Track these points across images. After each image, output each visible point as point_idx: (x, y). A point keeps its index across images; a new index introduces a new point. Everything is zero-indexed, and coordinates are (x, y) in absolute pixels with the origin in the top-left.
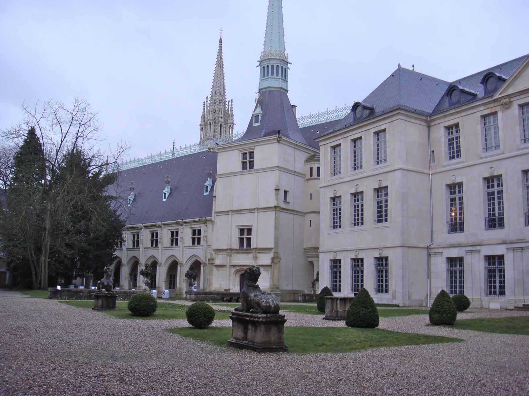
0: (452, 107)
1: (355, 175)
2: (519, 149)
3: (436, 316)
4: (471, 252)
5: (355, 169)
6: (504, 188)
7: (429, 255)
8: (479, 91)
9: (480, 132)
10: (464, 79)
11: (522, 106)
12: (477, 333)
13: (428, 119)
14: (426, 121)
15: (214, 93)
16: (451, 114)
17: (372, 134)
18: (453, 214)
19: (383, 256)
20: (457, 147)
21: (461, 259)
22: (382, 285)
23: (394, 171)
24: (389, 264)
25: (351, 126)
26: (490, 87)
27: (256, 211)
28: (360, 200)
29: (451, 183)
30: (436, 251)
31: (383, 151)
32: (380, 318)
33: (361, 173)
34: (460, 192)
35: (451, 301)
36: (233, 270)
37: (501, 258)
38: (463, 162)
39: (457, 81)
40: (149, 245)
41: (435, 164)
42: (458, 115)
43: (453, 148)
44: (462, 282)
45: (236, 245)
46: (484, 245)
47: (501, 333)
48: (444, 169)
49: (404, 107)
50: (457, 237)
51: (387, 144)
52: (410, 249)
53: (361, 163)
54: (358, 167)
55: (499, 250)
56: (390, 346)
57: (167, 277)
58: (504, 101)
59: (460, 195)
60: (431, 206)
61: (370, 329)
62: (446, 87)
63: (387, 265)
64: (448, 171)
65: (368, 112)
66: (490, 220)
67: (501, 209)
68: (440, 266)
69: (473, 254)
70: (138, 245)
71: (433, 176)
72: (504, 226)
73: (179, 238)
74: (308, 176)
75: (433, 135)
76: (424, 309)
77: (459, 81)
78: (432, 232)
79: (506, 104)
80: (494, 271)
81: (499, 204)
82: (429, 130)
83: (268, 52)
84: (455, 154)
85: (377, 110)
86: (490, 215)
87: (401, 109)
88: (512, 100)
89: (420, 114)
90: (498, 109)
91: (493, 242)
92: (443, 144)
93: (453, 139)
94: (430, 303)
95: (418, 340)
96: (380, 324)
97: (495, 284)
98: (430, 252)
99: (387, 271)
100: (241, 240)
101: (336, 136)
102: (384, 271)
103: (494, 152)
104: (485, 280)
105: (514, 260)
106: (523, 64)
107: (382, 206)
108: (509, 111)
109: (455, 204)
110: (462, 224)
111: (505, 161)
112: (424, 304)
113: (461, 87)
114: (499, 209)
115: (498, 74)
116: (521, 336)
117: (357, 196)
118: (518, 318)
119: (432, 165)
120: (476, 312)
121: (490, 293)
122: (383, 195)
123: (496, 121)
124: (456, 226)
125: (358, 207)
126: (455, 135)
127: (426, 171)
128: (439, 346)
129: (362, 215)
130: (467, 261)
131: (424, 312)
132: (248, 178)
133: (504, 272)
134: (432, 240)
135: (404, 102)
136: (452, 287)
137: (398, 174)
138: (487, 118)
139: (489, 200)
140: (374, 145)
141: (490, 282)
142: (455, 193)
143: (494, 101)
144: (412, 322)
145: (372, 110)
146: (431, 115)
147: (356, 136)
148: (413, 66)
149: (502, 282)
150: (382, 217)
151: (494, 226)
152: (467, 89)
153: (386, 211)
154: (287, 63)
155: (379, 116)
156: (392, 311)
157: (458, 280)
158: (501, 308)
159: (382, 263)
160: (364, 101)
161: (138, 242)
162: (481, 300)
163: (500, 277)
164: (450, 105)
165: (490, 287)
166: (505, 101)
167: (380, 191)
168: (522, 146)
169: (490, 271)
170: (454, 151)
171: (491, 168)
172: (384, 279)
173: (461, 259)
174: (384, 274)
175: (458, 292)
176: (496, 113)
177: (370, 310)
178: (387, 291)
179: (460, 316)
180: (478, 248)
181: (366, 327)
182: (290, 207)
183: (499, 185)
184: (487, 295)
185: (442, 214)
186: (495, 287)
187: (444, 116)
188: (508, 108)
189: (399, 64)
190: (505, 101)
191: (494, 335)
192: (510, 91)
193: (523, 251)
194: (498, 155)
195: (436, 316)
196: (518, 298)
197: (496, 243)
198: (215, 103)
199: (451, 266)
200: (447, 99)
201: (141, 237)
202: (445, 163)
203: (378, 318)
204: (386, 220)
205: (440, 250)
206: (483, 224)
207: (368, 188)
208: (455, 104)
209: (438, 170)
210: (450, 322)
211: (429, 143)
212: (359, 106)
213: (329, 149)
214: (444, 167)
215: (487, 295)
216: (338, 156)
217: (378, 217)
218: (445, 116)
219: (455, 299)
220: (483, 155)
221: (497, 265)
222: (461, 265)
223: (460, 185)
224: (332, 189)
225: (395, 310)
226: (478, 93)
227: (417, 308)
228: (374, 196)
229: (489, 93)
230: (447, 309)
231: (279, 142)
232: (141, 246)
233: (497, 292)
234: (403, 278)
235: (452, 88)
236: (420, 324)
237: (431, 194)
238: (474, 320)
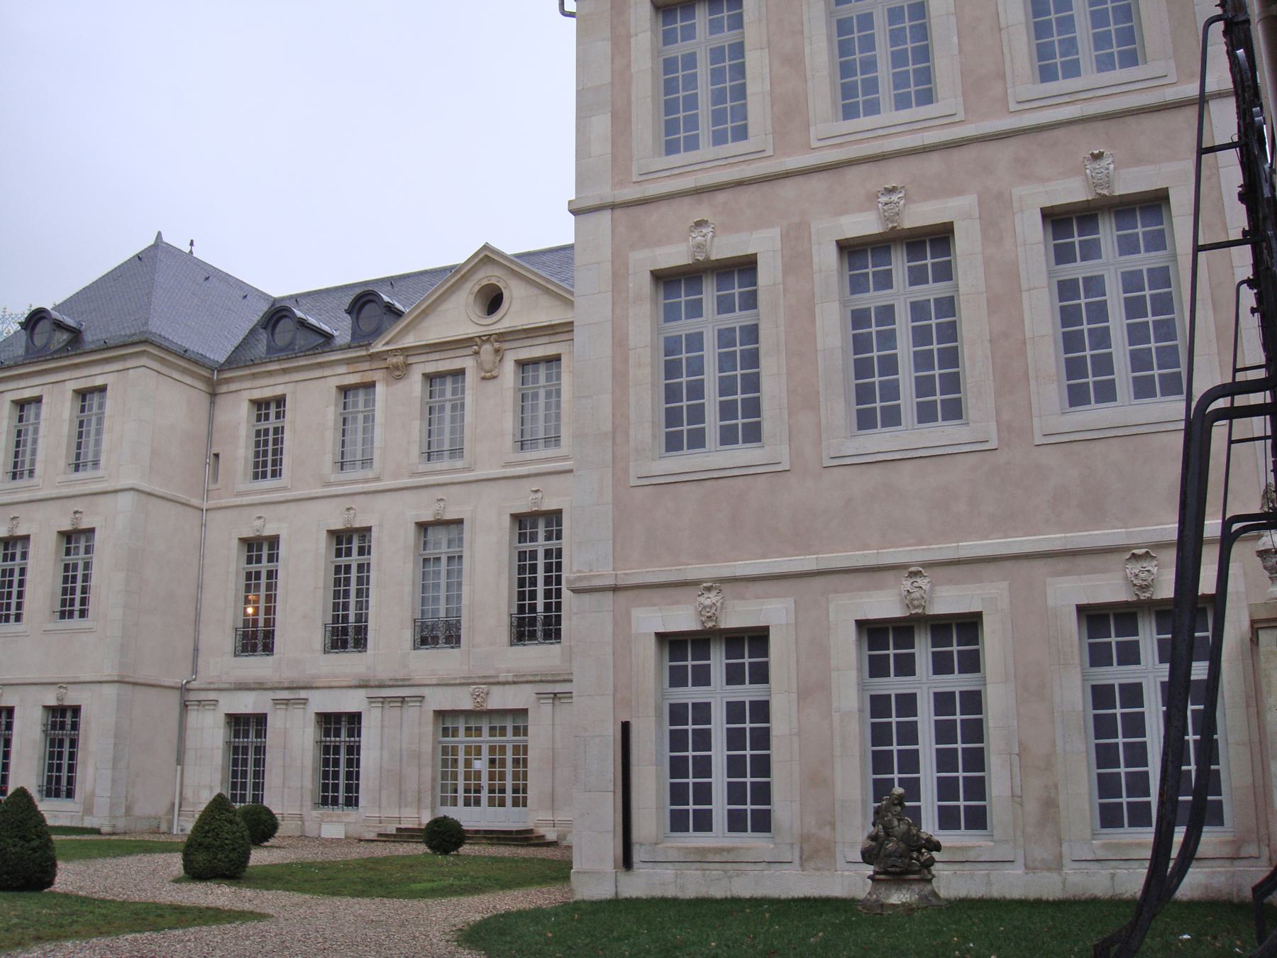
0: (274, 357)
2: (414, 474)
3: (201, 857)
4: (287, 702)
5: (14, 477)
6: (374, 558)
7: (185, 706)
8: (341, 328)
9: (331, 423)
10: (309, 294)
11: (430, 378)
12: (297, 897)
13: (212, 378)
14: (208, 381)
16: (270, 373)
17: (69, 394)
18: (250, 610)
19: (67, 703)
20: (275, 452)
21: (261, 719)
22: (59, 779)
23: (116, 491)
24: (82, 726)
25: (17, 365)
26: (366, 326)
28: (18, 556)
29: (251, 535)
31: (92, 442)
32: (61, 865)
34: (272, 558)
35: (238, 819)
37: (355, 718)
38: (285, 489)
39: (290, 297)
41: (218, 486)
42: (286, 378)
43: (265, 453)
44: (259, 774)
46: (317, 688)
47: (353, 896)
48: (239, 501)
49: (158, 340)
50: (256, 667)
51: (106, 423)
52: (138, 688)
53: (33, 462)
54: (22, 473)
56: (88, 936)
58: (393, 360)
59: (271, 566)
60: (200, 586)
61: (31, 894)
62: (264, 307)
63: (75, 726)
64: (246, 506)
65: (64, 337)
66: (335, 631)
67: (362, 605)
68: (209, 733)
69: (290, 707)
71: (211, 514)
72: (365, 646)
75: (222, 417)
76: (163, 838)
77: (296, 298)
78: (196, 650)
79: (396, 367)
80: (337, 750)
81: (359, 593)
82: (212, 403)
84: (269, 469)
85: (88, 337)
86: (336, 619)
87: (152, 343)
88: (411, 360)
89: (196, 363)
90: (377, 376)
91: (339, 682)
93: (266, 431)
94: (185, 825)
95: (160, 920)
96: (57, 879)
97: (338, 779)
98: (186, 698)
99: (73, 743)
102: (67, 744)
103: (359, 474)
104: (314, 770)
105: (382, 727)
106: (442, 285)
107: (74, 577)
108: (401, 385)
109: (258, 587)
110: (269, 635)
111: (380, 497)
112: (164, 828)
113: (299, 314)
114: (360, 605)
115: (386, 299)
116: (397, 903)
118: (386, 858)
119: (212, 487)
120: (291, 846)
121: (325, 801)
122: (82, 550)
123: (370, 403)
124: (256, 639)
125: (11, 574)
126: (272, 423)
127: (195, 501)
128: (211, 933)
129: (20, 595)
131: (167, 848)
133: (358, 754)
134: (195, 671)
135: (159, 326)
136: (234, 786)
137: (125, 500)
138: (351, 394)
139: (337, 582)
140: (71, 421)
141: (326, 775)
142: (259, 560)
143: (372, 357)
144: (137, 872)
145: (76, 335)
146: (221, 368)
147: (27, 394)
148: (192, 244)
149: (353, 776)
150: (72, 604)
151: (254, 649)
152: (312, 321)
156: (86, 843)
157: (250, 768)
158: (347, 837)
159: (63, 721)
160: (56, 308)
162: (301, 817)
163: (350, 763)
164: (270, 350)
165: (325, 788)
166: (394, 360)
168: (422, 468)
169: (326, 750)
170: (267, 459)
171: (348, 509)
172: (65, 762)
173: (261, 719)
174: (66, 750)
175: (249, 798)
176: (370, 386)
177: (35, 843)
178: (70, 794)
179: (259, 857)
180: (303, 694)
181: (21, 889)
183: (361, 551)
184: (316, 805)
185: (225, 607)
186: (336, 788)
187: (253, 374)
188: (399, 378)
189: (159, 234)
190: (394, 360)
191: (337, 900)
192: (409, 341)
193: (405, 706)
194: (366, 481)
195: (201, 857)
196: (386, 813)
197: (344, 684)
199: (237, 735)
200: (263, 336)
202: (241, 487)
203: (54, 865)
204: (83, 614)
205: (212, 695)
206: (318, 638)
208: (281, 350)
209: (224, 502)
210: (233, 871)
211: (210, 434)
212: (44, 318)
214: (239, 494)
215: (316, 805)
216: (31, 428)
217: (64, 603)
218: (254, 376)
219: (246, 813)
221: (344, 736)
222: (261, 733)
223: (274, 542)
225: (96, 844)
226: (336, 334)
227: (147, 838)
228: (58, 551)
229: (361, 337)
230: (227, 841)
233: (341, 800)
234: (116, 760)
235: (278, 314)
236: (158, 878)
237: (202, 557)
238: (288, 865)
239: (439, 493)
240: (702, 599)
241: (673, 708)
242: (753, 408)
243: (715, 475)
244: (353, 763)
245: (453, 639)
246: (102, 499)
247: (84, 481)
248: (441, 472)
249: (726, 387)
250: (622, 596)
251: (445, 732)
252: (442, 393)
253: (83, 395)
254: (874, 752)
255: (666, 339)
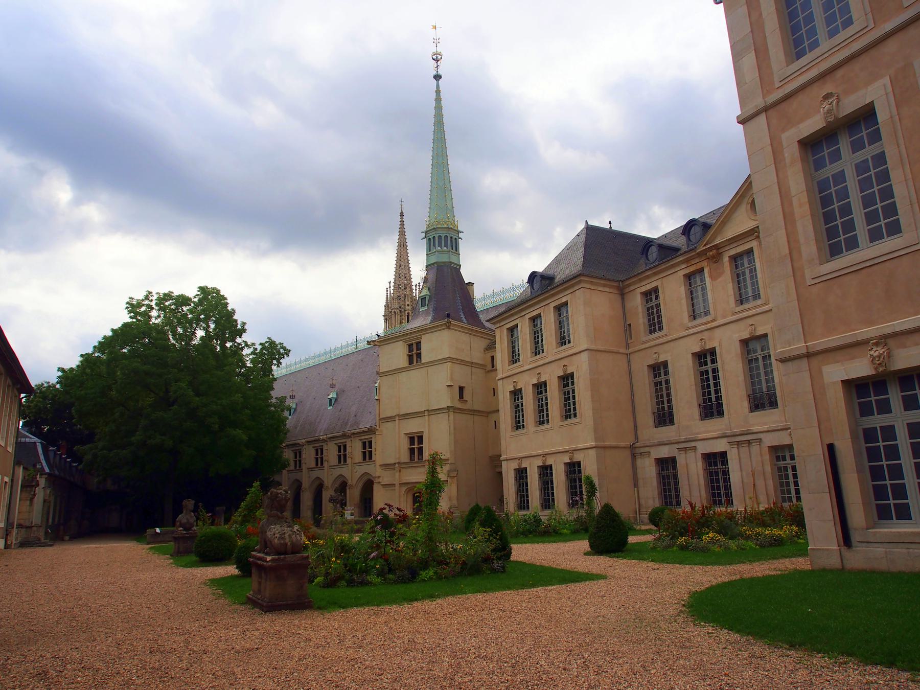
1: (536, 361)
2: (734, 313)
4: (685, 449)
7: (634, 456)
9: (684, 295)
11: (735, 259)
14: (618, 288)
15: (398, 276)
19: (574, 460)
21: (674, 460)
27: (426, 413)
30: (642, 450)
33: (542, 358)
36: (404, 488)
37: (723, 455)
38: (666, 335)
40: (313, 464)
43: (653, 319)
45: (405, 457)
48: (643, 346)
55: (720, 446)
57: (361, 501)
68: (648, 469)
70: (300, 466)
73: (373, 449)
74: (489, 367)
75: (628, 305)
79: (713, 257)
82: (623, 299)
83: (433, 220)
87: (583, 275)
90: (704, 264)
91: (710, 435)
92: (641, 315)
98: (634, 452)
100: (412, 451)
101: (512, 315)
103: (704, 319)
117: (540, 387)
124: (664, 417)
127: (621, 351)
130: (681, 460)
132: (416, 375)
134: (637, 438)
137: (585, 356)
147: (534, 313)
149: (728, 487)
153: (574, 403)
154: (459, 232)
155: (558, 286)
161: (300, 461)
167: (567, 379)
168: (738, 309)
169: (711, 474)
170: (655, 323)
173: (674, 460)
176: (701, 270)
180: (693, 444)
182: (468, 406)
194: (708, 322)
198: (399, 288)
201: (304, 456)
202: (644, 339)
205: (647, 449)
207: (551, 375)
213: (505, 331)
220: (690, 325)
224: (511, 380)
231: (448, 328)
232: (304, 467)
237: (631, 378)
239: (750, 321)
240: (872, 352)
241: (865, 431)
242: (891, 210)
243: (868, 264)
244: (727, 480)
245: (773, 404)
246: (574, 357)
247: (565, 350)
248: (749, 309)
249: (868, 201)
250: (815, 361)
251: (778, 458)
252: (743, 265)
253: (558, 308)
254: (870, 466)
255: (818, 183)
